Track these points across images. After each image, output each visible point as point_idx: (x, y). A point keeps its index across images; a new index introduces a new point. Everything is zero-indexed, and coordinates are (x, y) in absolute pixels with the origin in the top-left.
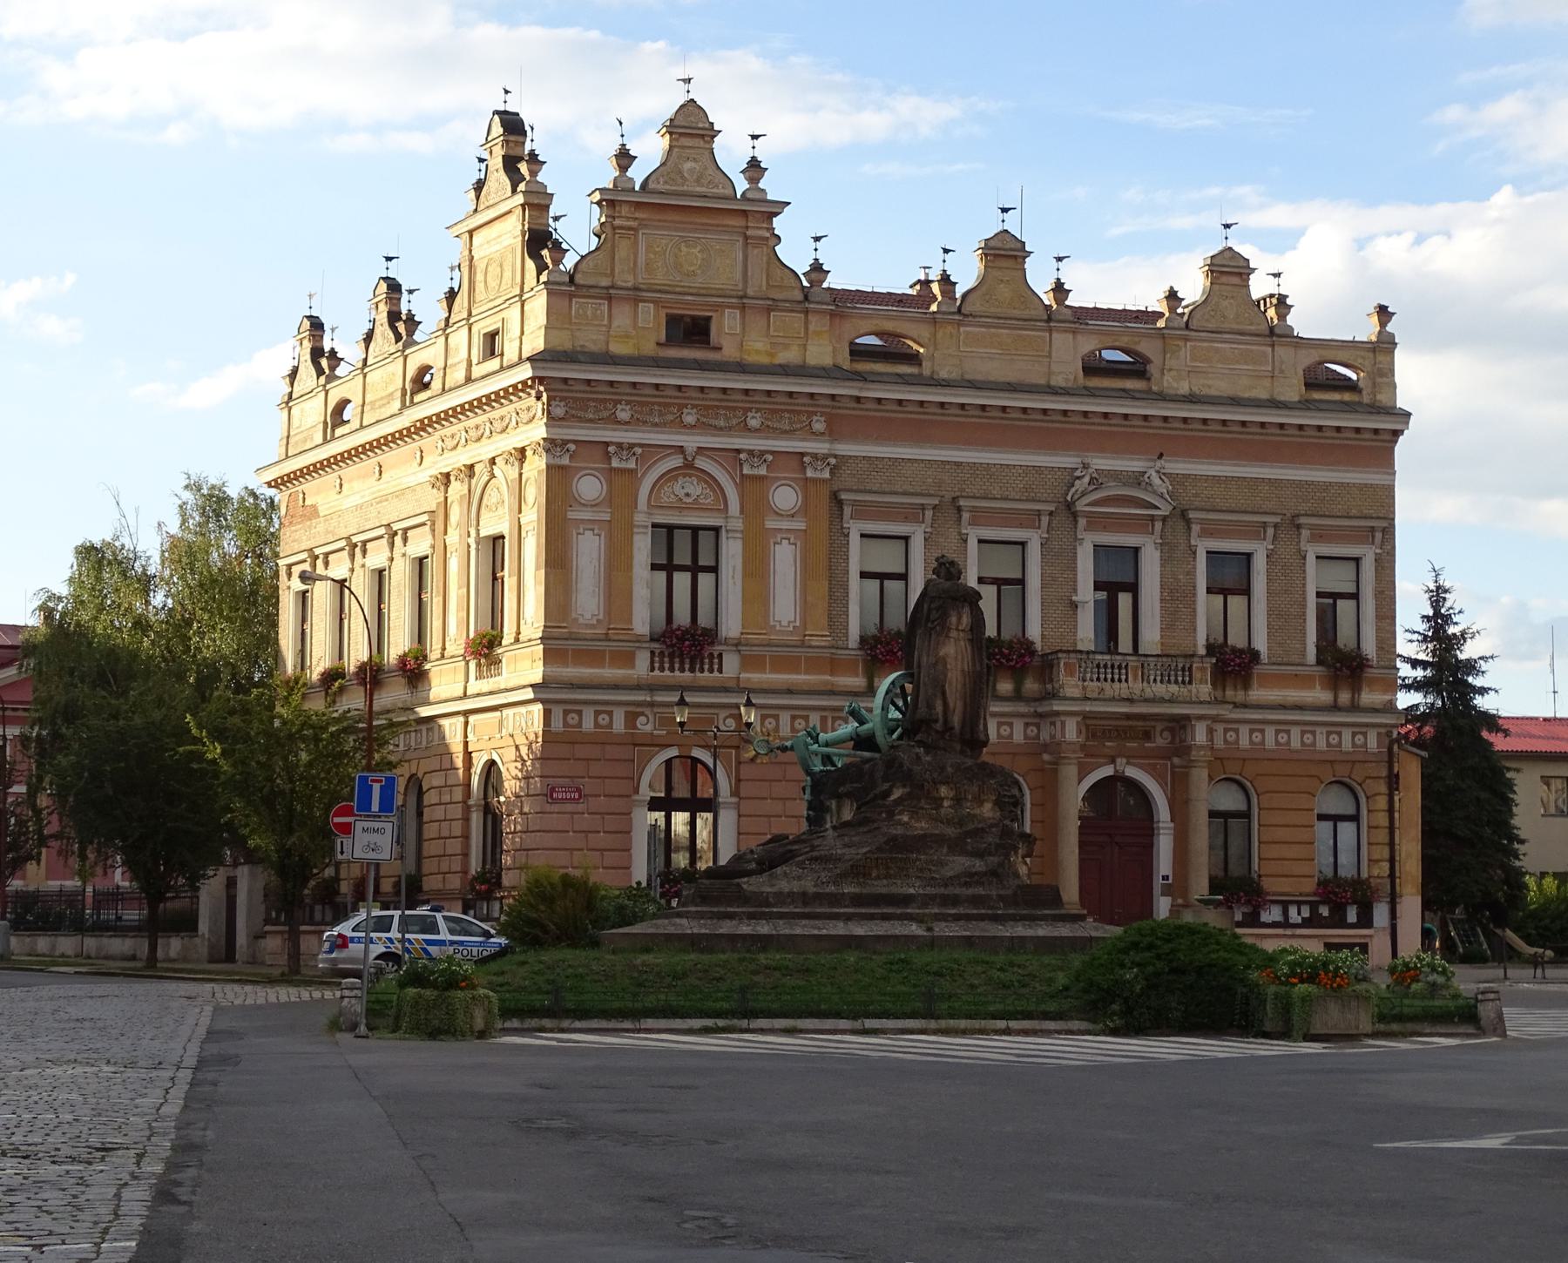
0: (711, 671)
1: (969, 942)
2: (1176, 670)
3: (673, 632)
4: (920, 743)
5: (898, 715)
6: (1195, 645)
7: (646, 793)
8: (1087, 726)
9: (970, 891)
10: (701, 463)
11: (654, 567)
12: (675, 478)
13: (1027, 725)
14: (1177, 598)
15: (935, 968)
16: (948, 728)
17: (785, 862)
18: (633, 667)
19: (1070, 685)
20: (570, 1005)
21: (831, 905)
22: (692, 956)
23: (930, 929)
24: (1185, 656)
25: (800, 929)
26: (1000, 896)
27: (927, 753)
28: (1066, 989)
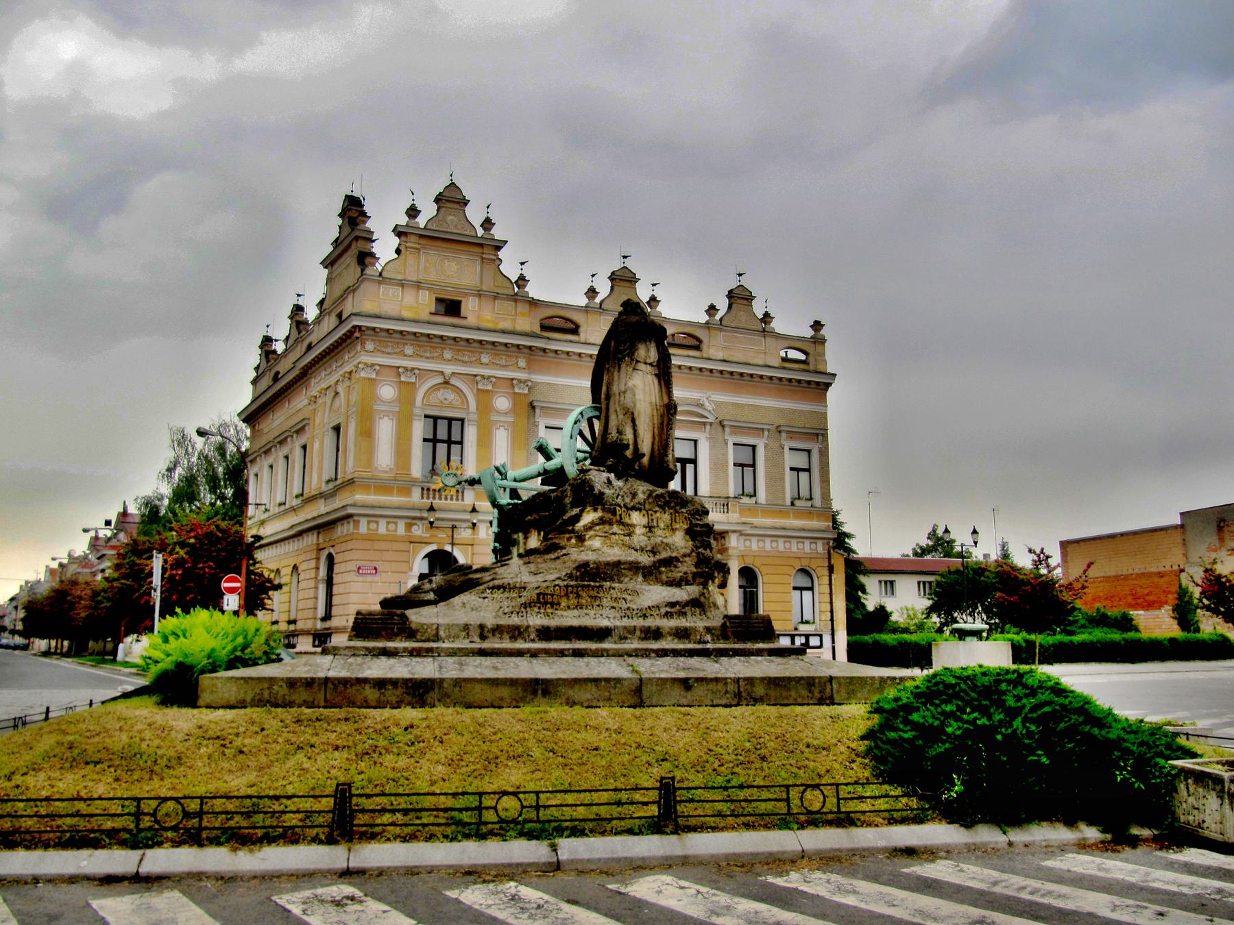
10: (454, 381)
11: (425, 440)
12: (438, 389)
16: (638, 455)
21: (513, 638)
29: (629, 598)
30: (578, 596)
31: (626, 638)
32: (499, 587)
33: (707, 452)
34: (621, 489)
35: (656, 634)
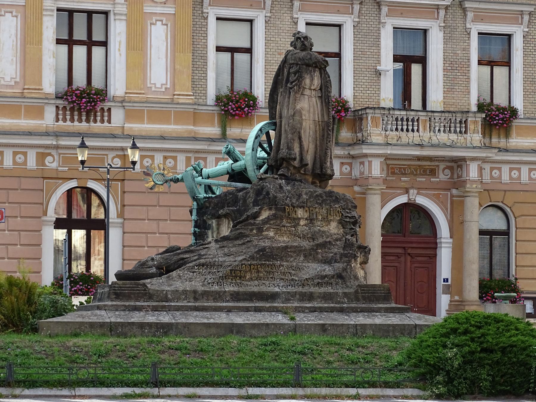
0: (102, 121)
1: (323, 328)
2: (455, 123)
3: (73, 91)
4: (282, 176)
5: (263, 154)
6: (469, 104)
7: (52, 216)
8: (388, 165)
9: (323, 290)
11: (59, 42)
13: (342, 164)
14: (455, 68)
15: (300, 348)
17: (179, 267)
18: (42, 118)
19: (375, 133)
20: (21, 377)
21: (215, 300)
22: (111, 340)
23: (292, 319)
24: (462, 112)
25: (194, 318)
26: (345, 294)
27: (288, 184)
28: (400, 364)
29: (293, 272)
30: (258, 272)
31: (290, 300)
32: (203, 265)
33: (441, 46)
34: (289, 192)
35: (311, 297)
